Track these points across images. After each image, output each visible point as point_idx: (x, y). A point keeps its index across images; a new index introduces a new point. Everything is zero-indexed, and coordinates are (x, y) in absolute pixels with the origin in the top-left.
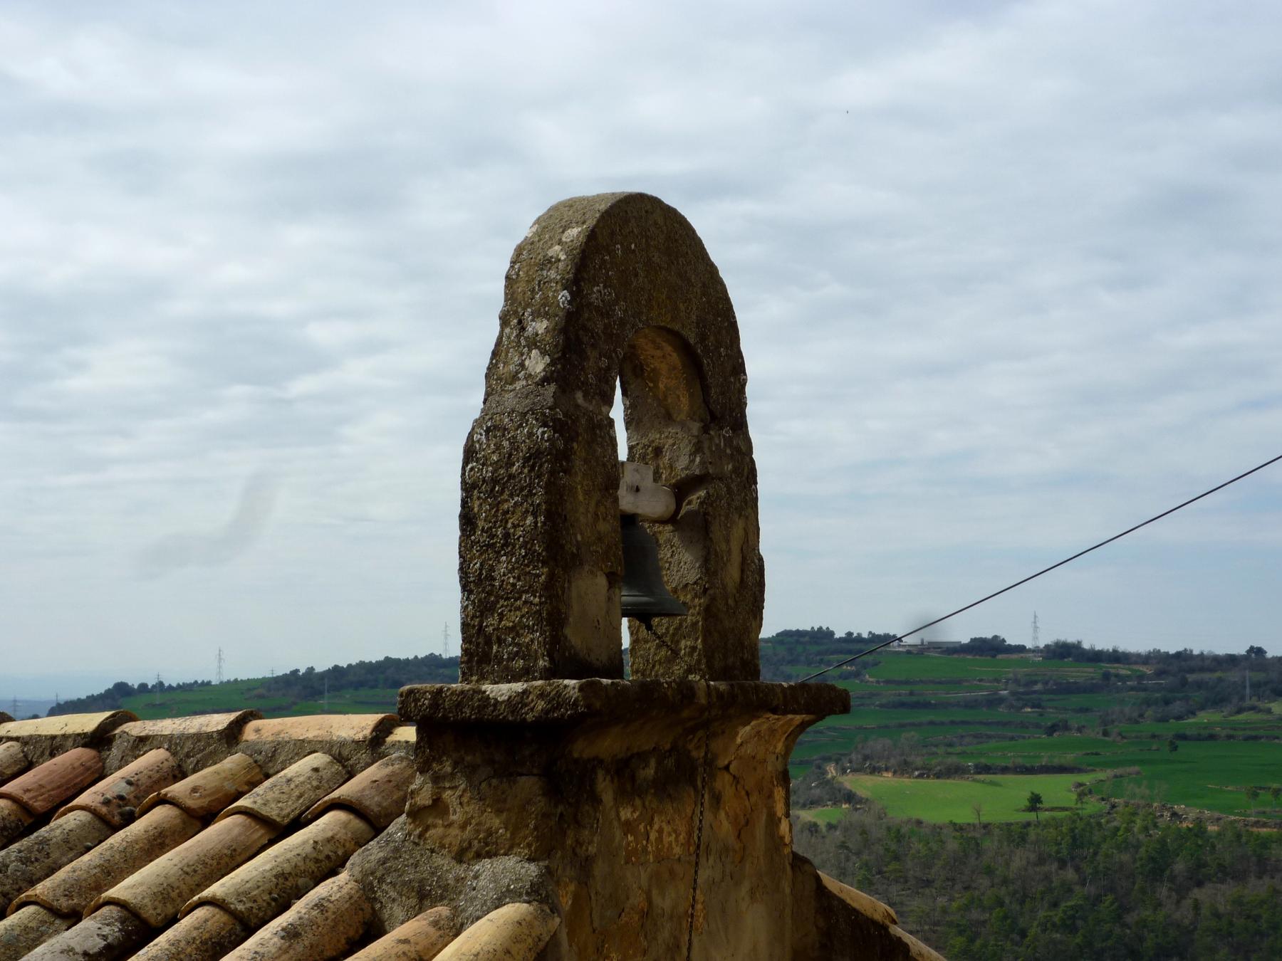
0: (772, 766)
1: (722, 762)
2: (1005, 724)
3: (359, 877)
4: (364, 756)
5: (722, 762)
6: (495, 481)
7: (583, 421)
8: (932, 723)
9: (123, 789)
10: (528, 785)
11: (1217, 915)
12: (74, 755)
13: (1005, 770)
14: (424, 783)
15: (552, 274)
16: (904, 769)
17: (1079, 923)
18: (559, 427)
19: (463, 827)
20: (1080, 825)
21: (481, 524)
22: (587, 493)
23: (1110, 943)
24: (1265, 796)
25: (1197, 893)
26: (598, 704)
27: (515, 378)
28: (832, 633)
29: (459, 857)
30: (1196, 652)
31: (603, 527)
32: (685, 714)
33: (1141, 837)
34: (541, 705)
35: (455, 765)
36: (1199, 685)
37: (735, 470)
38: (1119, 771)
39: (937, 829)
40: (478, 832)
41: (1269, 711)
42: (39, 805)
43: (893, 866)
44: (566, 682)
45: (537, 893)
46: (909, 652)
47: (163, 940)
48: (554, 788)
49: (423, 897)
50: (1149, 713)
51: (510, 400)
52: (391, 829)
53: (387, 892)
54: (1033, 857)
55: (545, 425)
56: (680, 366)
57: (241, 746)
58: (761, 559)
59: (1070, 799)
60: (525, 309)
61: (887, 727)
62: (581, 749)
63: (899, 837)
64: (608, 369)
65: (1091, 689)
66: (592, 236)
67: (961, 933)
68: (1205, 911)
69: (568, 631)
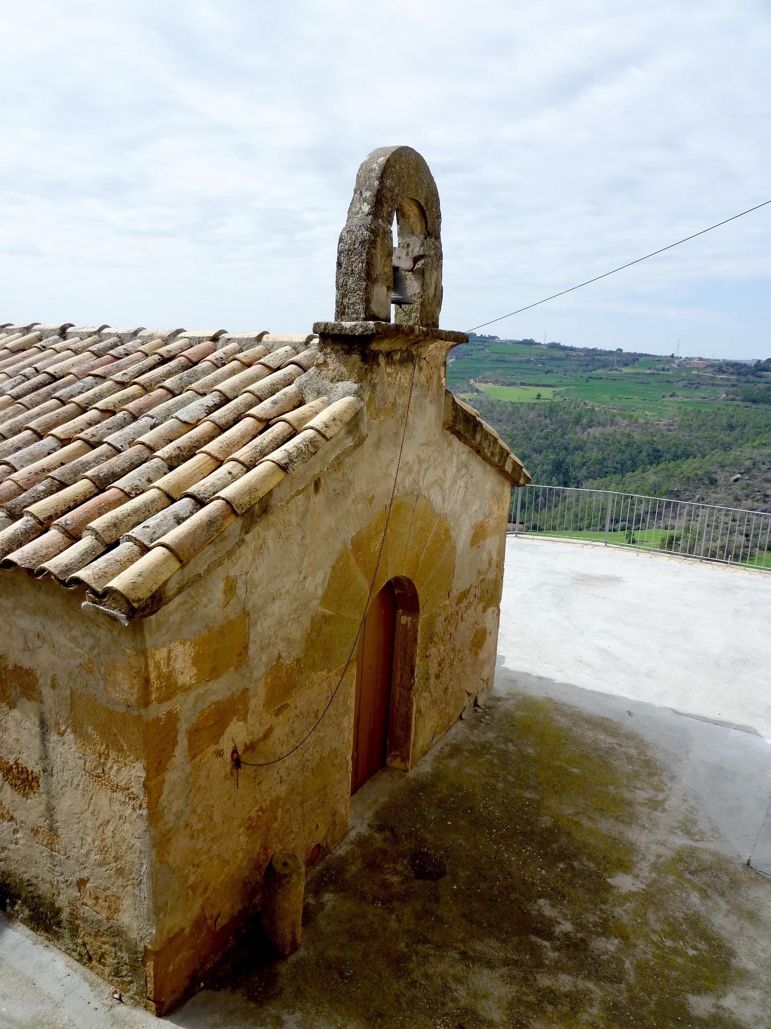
0: (441, 360)
1: (423, 356)
2: (531, 369)
3: (298, 386)
4: (303, 348)
5: (423, 356)
6: (349, 250)
7: (381, 230)
8: (507, 367)
9: (222, 355)
10: (356, 357)
11: (595, 438)
12: (207, 344)
13: (530, 385)
14: (321, 355)
15: (373, 174)
16: (496, 382)
17: (549, 437)
18: (373, 232)
19: (333, 371)
20: (553, 405)
21: (343, 266)
22: (381, 257)
23: (559, 444)
24: (616, 399)
25: (589, 430)
26: (380, 331)
27: (358, 213)
28: (476, 335)
29: (332, 381)
30: (599, 349)
31: (386, 270)
32: (411, 337)
33: (573, 410)
34: (361, 330)
35: (332, 349)
36: (599, 360)
37: (435, 254)
38: (567, 388)
39: (505, 403)
40: (338, 373)
41: (621, 371)
42: (194, 359)
43: (490, 414)
44: (370, 322)
45: (357, 394)
46: (501, 343)
47: (232, 403)
48: (364, 360)
49: (319, 394)
50: (580, 369)
51: (356, 221)
52: (309, 371)
53: (307, 391)
54: (536, 415)
55: (367, 230)
56: (418, 214)
57: (262, 343)
58: (442, 287)
59: (550, 396)
60: (362, 188)
61: (491, 368)
62: (374, 346)
63: (493, 405)
64: (391, 211)
65: (561, 359)
66: (388, 161)
67: (510, 438)
68: (591, 436)
69: (372, 305)
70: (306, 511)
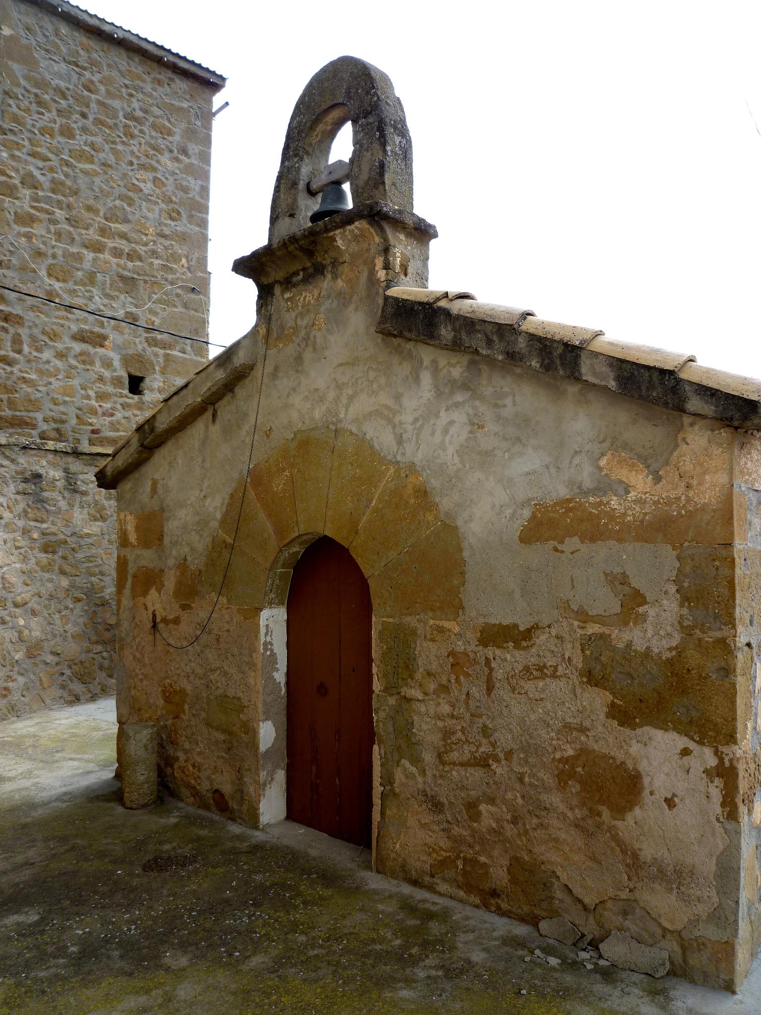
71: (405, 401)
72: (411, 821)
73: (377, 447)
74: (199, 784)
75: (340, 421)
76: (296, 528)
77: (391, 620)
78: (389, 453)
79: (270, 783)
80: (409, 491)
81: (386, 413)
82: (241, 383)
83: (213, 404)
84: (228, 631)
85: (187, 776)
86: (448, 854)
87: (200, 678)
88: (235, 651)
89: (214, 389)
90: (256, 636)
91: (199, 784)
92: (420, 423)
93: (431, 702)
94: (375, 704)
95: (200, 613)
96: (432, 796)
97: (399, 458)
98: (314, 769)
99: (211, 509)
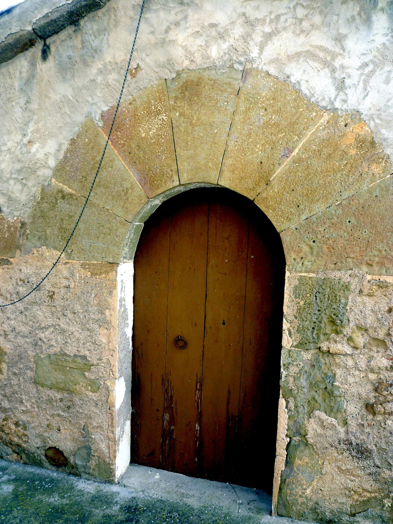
70: (32, 76)
71: (350, 43)
72: (327, 468)
73: (306, 91)
74: (26, 442)
75: (251, 61)
76: (176, 178)
77: (312, 275)
78: (324, 99)
79: (122, 437)
80: (350, 139)
81: (321, 55)
82: (91, 15)
83: (43, 38)
84: (68, 287)
85: (8, 434)
86: (373, 495)
87: (24, 337)
88: (78, 308)
89: (55, 16)
90: (111, 293)
91: (26, 442)
92: (371, 67)
93: (361, 356)
94: (284, 359)
95: (24, 269)
96: (357, 444)
97: (338, 105)
98: (167, 417)
99: (40, 156)
